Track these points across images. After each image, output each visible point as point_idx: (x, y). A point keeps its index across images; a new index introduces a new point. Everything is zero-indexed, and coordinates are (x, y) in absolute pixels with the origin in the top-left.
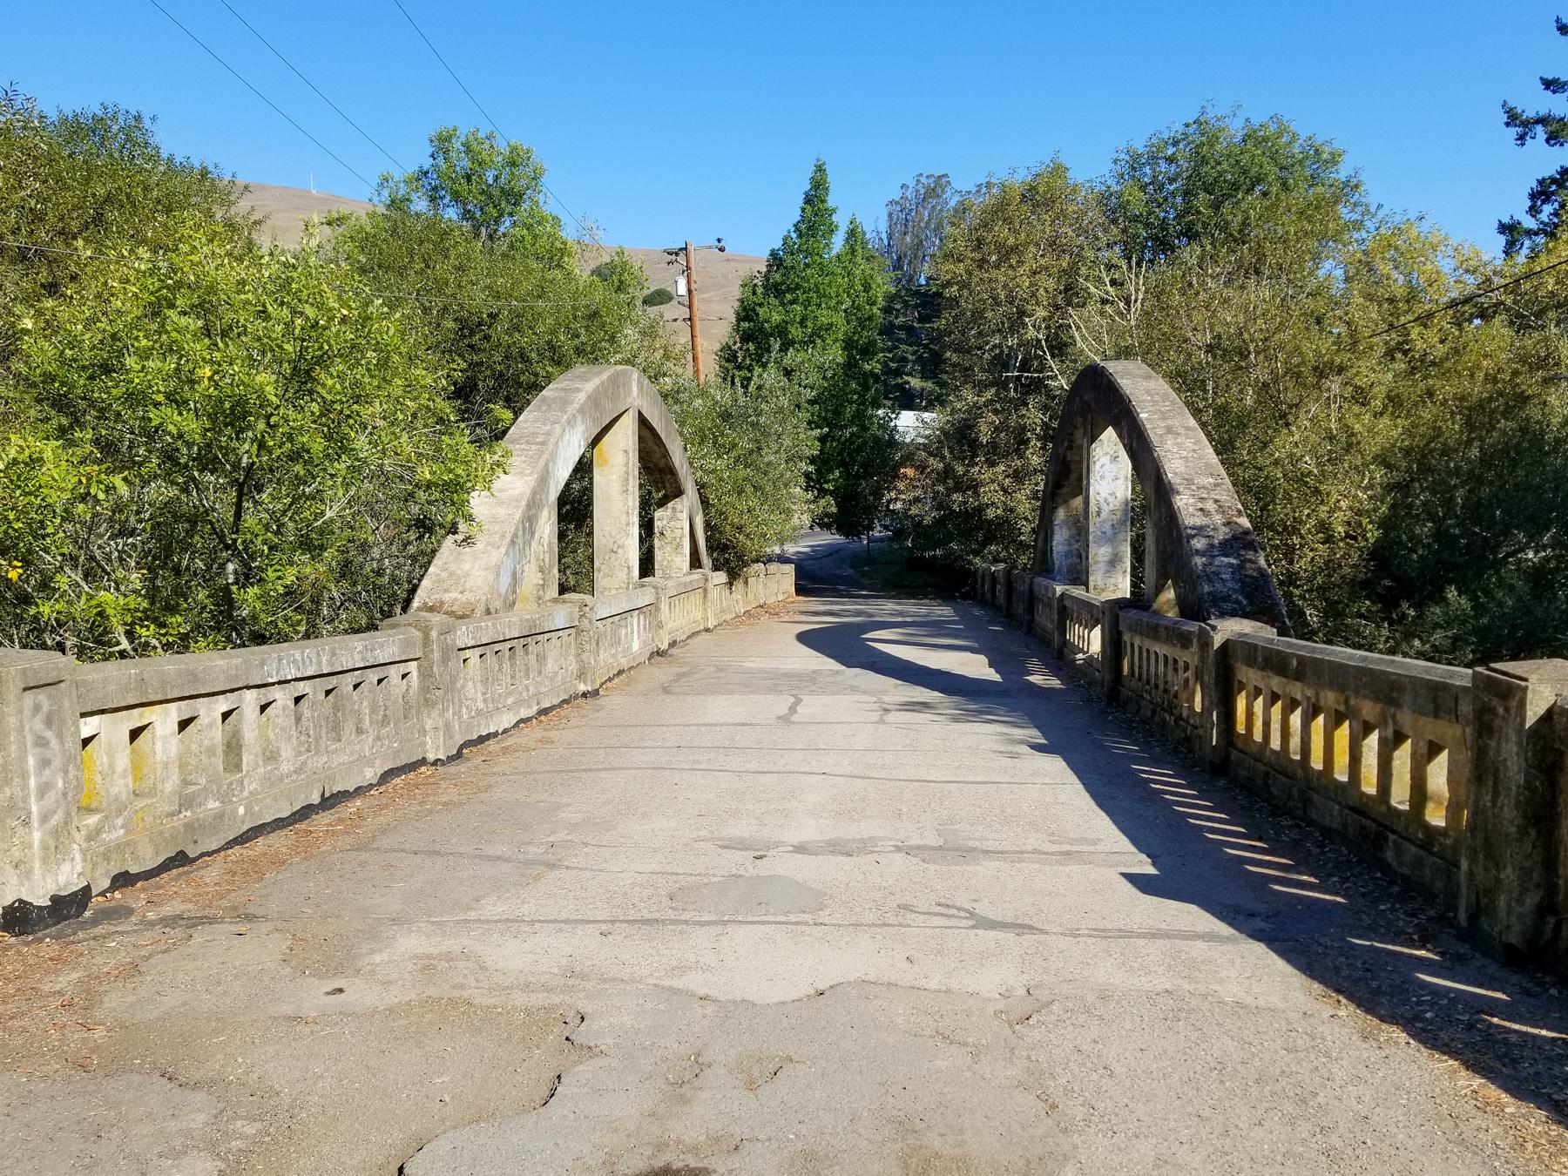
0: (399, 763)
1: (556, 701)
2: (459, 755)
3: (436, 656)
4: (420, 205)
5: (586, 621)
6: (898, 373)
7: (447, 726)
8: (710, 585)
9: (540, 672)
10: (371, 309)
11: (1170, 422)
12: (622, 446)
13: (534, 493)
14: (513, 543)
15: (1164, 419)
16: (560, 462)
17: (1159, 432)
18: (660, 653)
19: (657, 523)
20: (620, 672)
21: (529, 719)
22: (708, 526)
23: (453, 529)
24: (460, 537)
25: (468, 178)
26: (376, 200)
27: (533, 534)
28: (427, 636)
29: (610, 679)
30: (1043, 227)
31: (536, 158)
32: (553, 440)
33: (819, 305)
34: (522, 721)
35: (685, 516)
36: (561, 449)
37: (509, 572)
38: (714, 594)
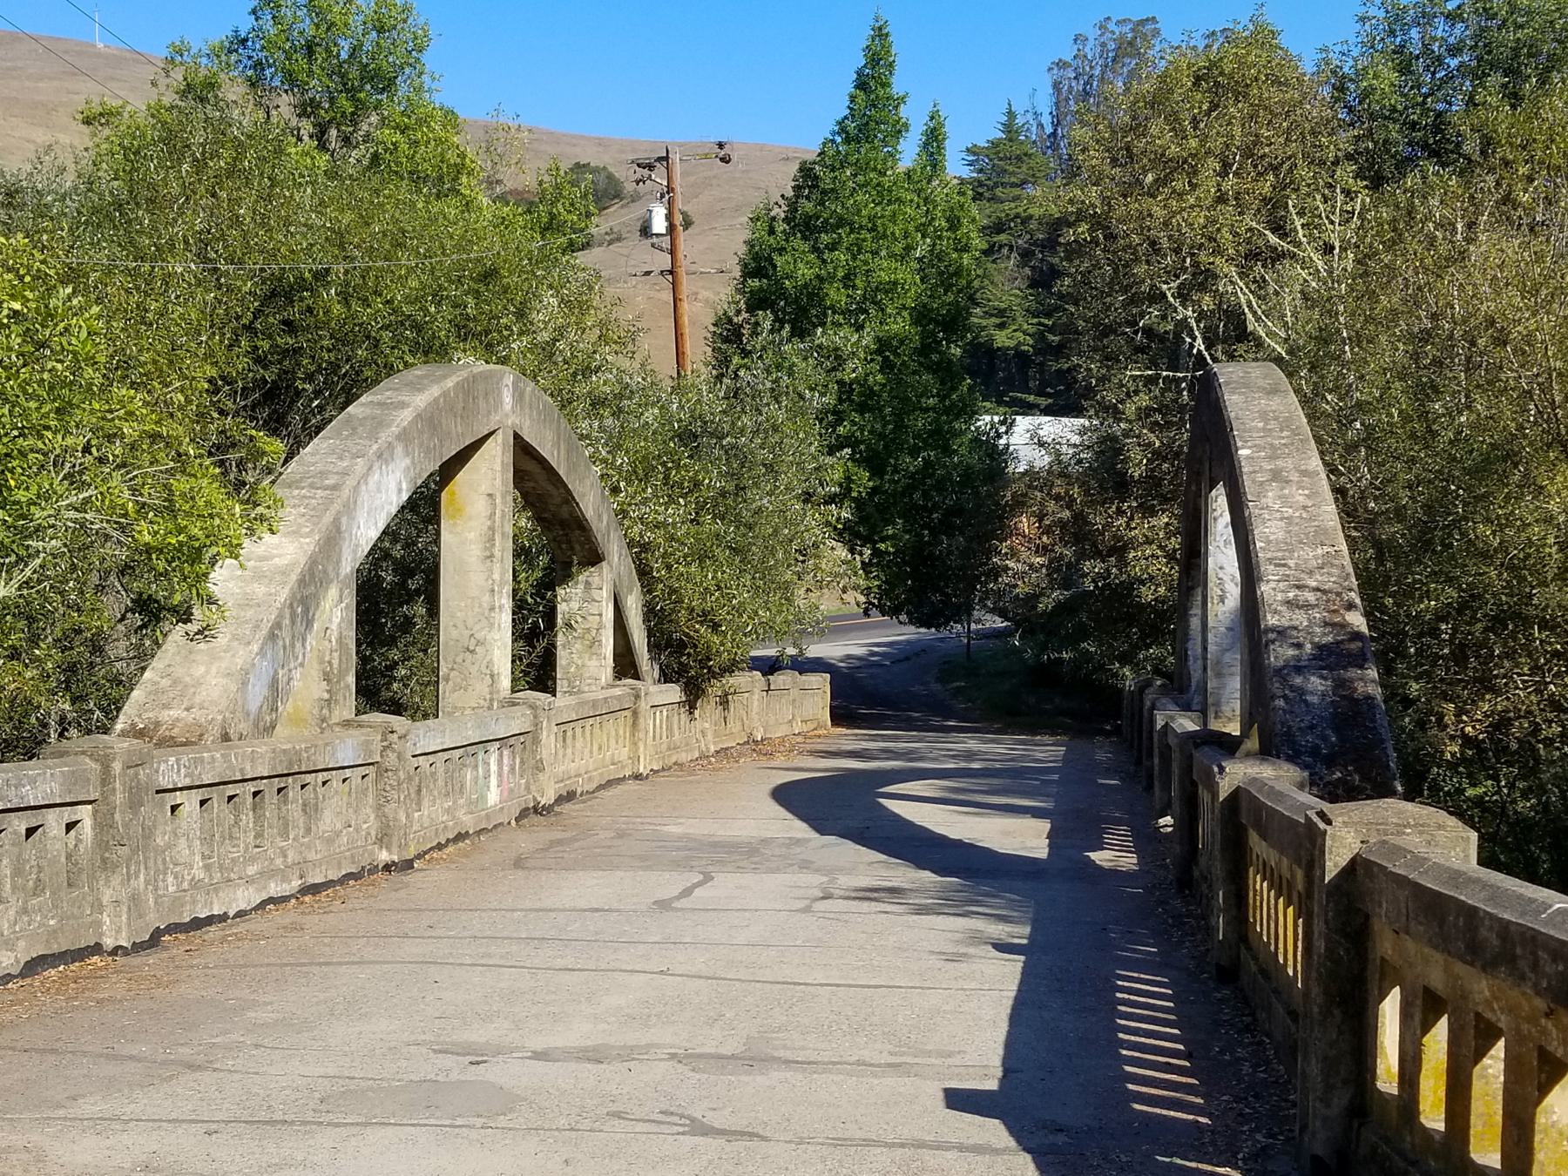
0: (55, 948)
1: (334, 875)
2: (154, 940)
3: (119, 798)
4: (234, 90)
5: (392, 756)
6: (1059, 351)
7: (135, 899)
8: (644, 705)
9: (308, 830)
10: (53, 303)
11: (1280, 463)
12: (485, 488)
13: (313, 561)
14: (272, 637)
15: (1272, 458)
16: (362, 517)
17: (1260, 478)
18: (537, 810)
19: (562, 608)
20: (460, 837)
21: (284, 899)
22: (650, 612)
23: (186, 618)
24: (193, 627)
25: (310, 48)
26: (162, 82)
27: (309, 624)
28: (106, 769)
29: (440, 847)
30: (1233, 126)
31: (418, 18)
32: (350, 482)
33: (875, 253)
34: (271, 900)
35: (605, 595)
36: (364, 496)
37: (266, 679)
38: (649, 722)
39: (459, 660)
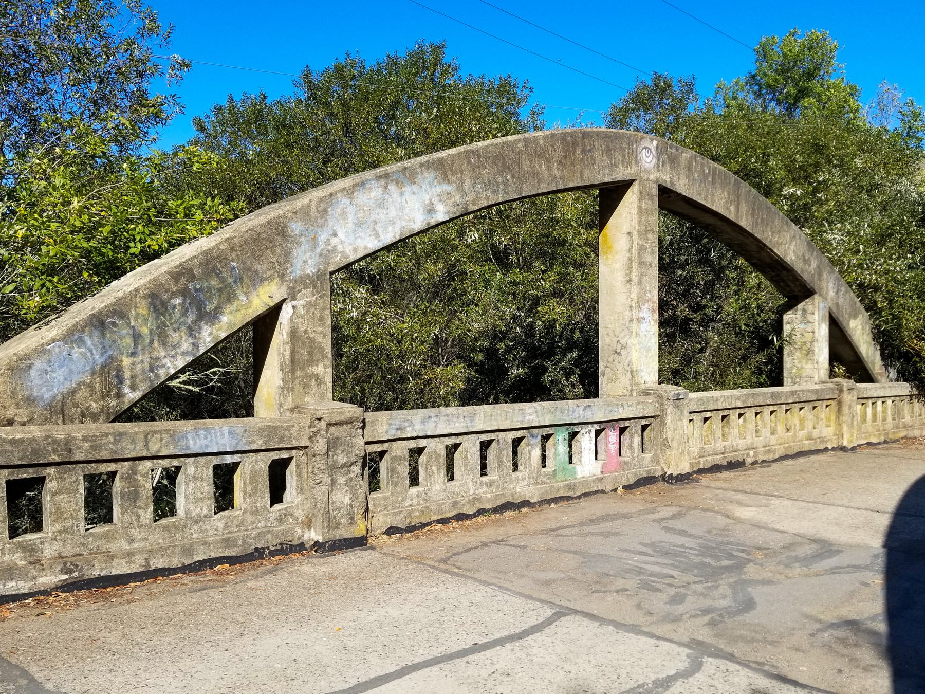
1: (175, 563)
12: (626, 229)
39: (611, 360)
